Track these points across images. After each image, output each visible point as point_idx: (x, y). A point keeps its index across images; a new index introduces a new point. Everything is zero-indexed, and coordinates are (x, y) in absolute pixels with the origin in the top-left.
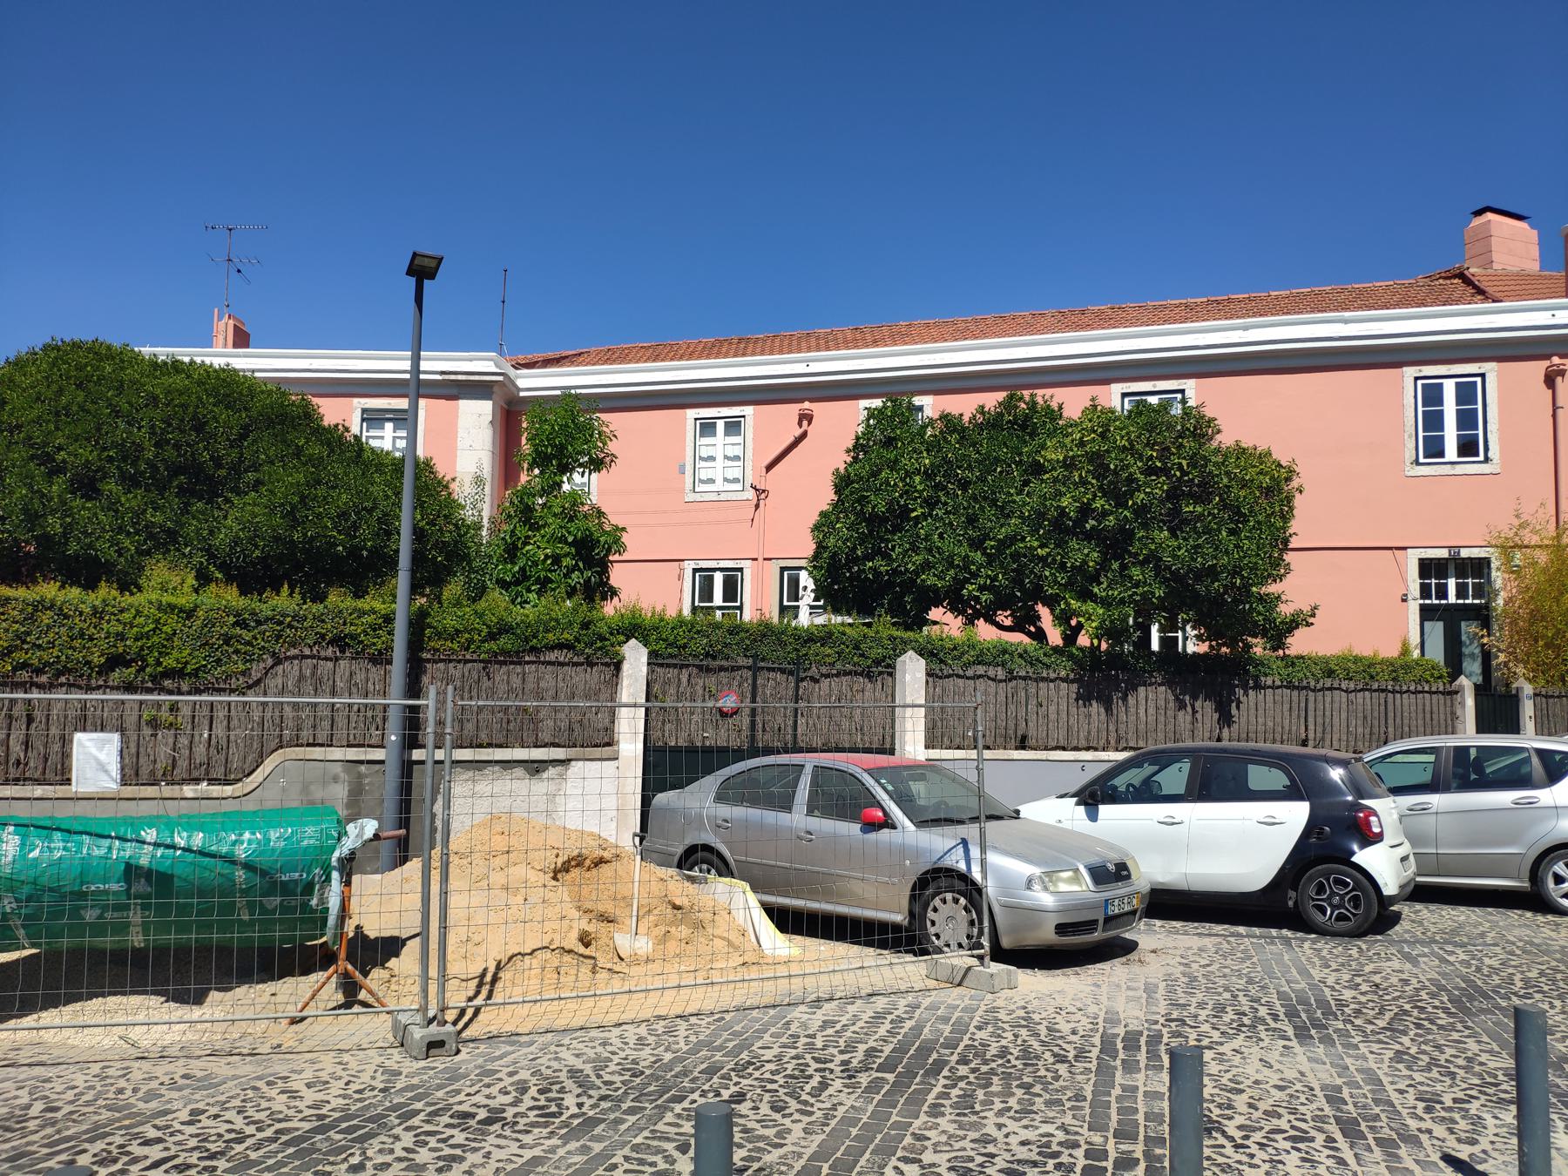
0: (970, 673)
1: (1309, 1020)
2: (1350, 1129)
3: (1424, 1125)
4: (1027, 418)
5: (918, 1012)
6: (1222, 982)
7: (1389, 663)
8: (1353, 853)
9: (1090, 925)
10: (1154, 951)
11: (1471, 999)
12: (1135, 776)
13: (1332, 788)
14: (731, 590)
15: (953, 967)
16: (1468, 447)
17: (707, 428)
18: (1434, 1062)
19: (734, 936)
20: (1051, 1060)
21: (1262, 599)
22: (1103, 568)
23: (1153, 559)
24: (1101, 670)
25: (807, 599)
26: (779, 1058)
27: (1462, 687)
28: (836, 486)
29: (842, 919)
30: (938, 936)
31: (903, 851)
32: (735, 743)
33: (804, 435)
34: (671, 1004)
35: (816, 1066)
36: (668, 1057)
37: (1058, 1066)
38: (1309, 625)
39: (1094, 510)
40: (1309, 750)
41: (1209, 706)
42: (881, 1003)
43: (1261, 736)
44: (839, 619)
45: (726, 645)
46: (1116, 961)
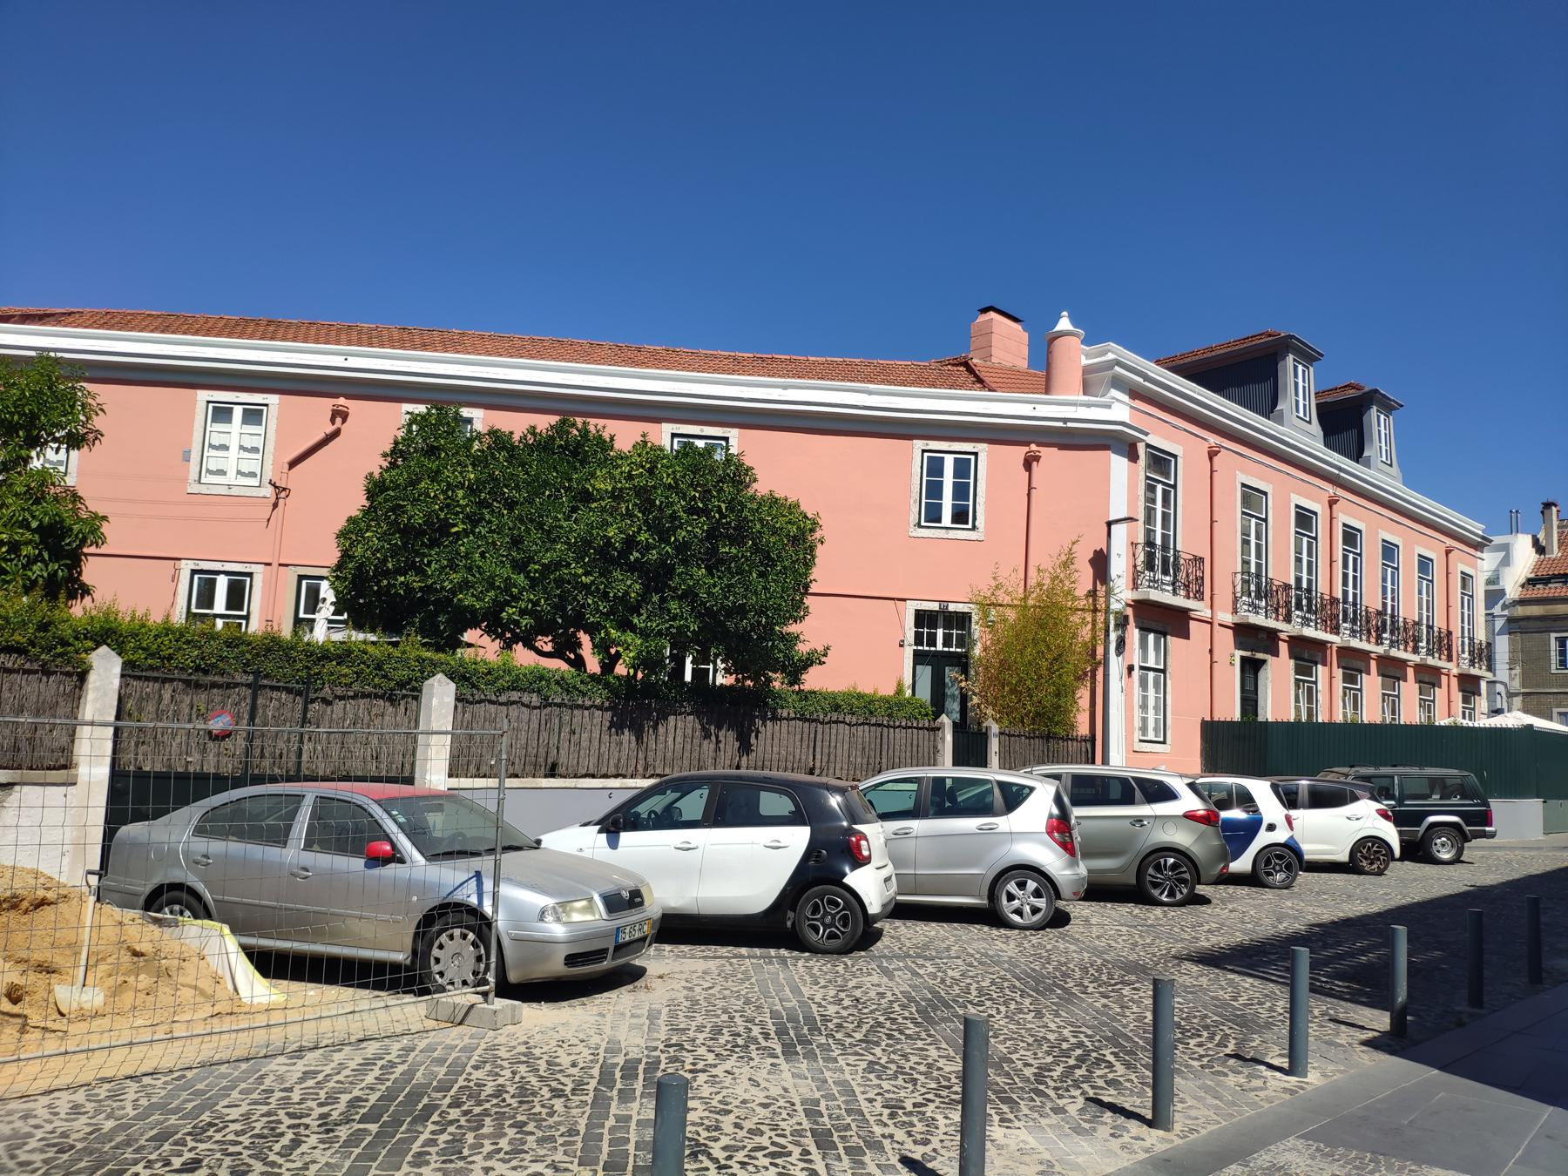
0: (503, 699)
1: (796, 1037)
2: (824, 1141)
3: (887, 1131)
4: (579, 445)
5: (413, 1055)
6: (721, 1004)
7: (885, 700)
8: (845, 875)
9: (599, 954)
10: (660, 977)
11: (935, 1009)
12: (657, 803)
13: (830, 814)
14: (237, 595)
15: (455, 1006)
16: (960, 516)
17: (222, 413)
18: (900, 1070)
19: (205, 984)
20: (548, 1095)
21: (783, 637)
22: (643, 600)
23: (689, 596)
24: (635, 699)
25: (326, 611)
26: (246, 1117)
27: (943, 724)
28: (368, 491)
29: (334, 961)
30: (441, 974)
31: (410, 886)
32: (228, 767)
33: (337, 433)
34: (118, 1063)
35: (288, 1121)
36: (110, 1124)
37: (554, 1101)
38: (821, 663)
39: (639, 543)
40: (814, 779)
41: (731, 735)
42: (371, 1049)
43: (775, 764)
44: (361, 636)
45: (222, 659)
46: (623, 989)
